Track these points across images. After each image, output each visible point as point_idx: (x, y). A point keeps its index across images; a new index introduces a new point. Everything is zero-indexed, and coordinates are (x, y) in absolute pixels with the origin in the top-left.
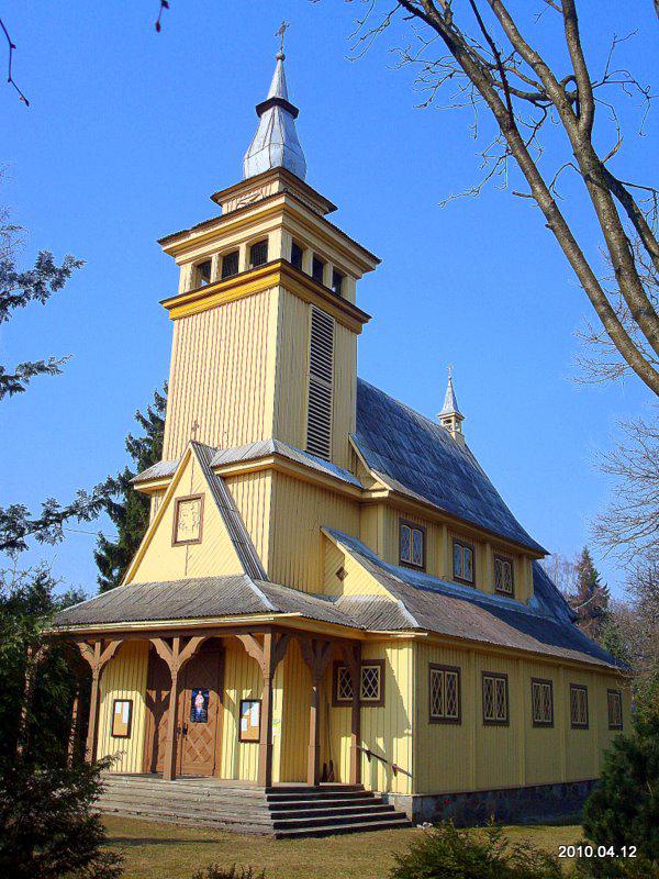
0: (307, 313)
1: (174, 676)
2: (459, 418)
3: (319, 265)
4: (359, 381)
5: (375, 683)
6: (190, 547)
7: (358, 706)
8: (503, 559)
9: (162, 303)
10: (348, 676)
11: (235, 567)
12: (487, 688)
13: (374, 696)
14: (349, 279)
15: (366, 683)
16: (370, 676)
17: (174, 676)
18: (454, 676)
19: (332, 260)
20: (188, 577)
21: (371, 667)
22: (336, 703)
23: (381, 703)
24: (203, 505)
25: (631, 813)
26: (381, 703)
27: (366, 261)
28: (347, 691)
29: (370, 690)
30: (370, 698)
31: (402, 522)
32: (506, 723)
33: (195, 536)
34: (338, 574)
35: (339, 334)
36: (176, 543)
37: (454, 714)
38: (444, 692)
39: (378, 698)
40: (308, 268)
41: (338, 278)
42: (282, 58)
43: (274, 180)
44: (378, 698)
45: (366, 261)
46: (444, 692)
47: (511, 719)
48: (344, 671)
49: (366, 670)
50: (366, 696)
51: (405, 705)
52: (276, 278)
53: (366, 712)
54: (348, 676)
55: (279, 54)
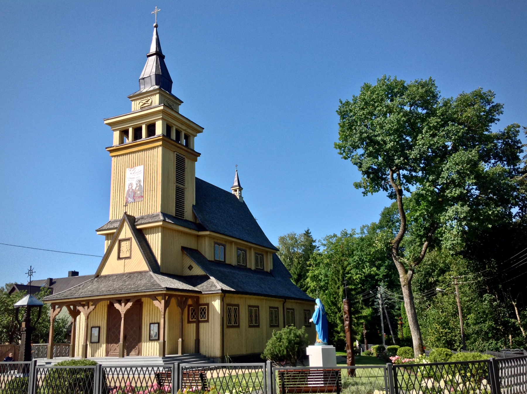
0: (173, 157)
1: (123, 316)
2: (241, 189)
3: (178, 133)
4: (196, 178)
5: (205, 313)
6: (126, 260)
7: (198, 323)
8: (259, 254)
9: (106, 148)
10: (194, 311)
11: (144, 266)
12: (250, 312)
13: (205, 318)
14: (191, 138)
15: (201, 313)
16: (203, 310)
17: (123, 316)
18: (236, 308)
19: (183, 130)
20: (125, 272)
21: (203, 307)
22: (189, 322)
23: (207, 321)
24: (131, 242)
25: (392, 236)
26: (207, 321)
27: (199, 129)
28: (194, 317)
29: (203, 316)
30: (203, 319)
31: (216, 243)
32: (258, 326)
33: (128, 255)
34: (189, 268)
35: (187, 162)
36: (119, 258)
37: (237, 324)
38: (233, 314)
39: (206, 319)
40: (173, 136)
41: (187, 137)
42: (156, 26)
43: (157, 94)
44: (206, 319)
45: (199, 129)
46: (233, 314)
47: (260, 324)
48: (192, 309)
49: (201, 308)
50: (201, 318)
51: (217, 309)
52: (160, 143)
53: (202, 325)
54: (194, 311)
55: (155, 25)
